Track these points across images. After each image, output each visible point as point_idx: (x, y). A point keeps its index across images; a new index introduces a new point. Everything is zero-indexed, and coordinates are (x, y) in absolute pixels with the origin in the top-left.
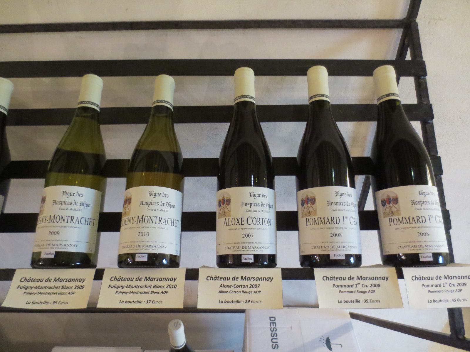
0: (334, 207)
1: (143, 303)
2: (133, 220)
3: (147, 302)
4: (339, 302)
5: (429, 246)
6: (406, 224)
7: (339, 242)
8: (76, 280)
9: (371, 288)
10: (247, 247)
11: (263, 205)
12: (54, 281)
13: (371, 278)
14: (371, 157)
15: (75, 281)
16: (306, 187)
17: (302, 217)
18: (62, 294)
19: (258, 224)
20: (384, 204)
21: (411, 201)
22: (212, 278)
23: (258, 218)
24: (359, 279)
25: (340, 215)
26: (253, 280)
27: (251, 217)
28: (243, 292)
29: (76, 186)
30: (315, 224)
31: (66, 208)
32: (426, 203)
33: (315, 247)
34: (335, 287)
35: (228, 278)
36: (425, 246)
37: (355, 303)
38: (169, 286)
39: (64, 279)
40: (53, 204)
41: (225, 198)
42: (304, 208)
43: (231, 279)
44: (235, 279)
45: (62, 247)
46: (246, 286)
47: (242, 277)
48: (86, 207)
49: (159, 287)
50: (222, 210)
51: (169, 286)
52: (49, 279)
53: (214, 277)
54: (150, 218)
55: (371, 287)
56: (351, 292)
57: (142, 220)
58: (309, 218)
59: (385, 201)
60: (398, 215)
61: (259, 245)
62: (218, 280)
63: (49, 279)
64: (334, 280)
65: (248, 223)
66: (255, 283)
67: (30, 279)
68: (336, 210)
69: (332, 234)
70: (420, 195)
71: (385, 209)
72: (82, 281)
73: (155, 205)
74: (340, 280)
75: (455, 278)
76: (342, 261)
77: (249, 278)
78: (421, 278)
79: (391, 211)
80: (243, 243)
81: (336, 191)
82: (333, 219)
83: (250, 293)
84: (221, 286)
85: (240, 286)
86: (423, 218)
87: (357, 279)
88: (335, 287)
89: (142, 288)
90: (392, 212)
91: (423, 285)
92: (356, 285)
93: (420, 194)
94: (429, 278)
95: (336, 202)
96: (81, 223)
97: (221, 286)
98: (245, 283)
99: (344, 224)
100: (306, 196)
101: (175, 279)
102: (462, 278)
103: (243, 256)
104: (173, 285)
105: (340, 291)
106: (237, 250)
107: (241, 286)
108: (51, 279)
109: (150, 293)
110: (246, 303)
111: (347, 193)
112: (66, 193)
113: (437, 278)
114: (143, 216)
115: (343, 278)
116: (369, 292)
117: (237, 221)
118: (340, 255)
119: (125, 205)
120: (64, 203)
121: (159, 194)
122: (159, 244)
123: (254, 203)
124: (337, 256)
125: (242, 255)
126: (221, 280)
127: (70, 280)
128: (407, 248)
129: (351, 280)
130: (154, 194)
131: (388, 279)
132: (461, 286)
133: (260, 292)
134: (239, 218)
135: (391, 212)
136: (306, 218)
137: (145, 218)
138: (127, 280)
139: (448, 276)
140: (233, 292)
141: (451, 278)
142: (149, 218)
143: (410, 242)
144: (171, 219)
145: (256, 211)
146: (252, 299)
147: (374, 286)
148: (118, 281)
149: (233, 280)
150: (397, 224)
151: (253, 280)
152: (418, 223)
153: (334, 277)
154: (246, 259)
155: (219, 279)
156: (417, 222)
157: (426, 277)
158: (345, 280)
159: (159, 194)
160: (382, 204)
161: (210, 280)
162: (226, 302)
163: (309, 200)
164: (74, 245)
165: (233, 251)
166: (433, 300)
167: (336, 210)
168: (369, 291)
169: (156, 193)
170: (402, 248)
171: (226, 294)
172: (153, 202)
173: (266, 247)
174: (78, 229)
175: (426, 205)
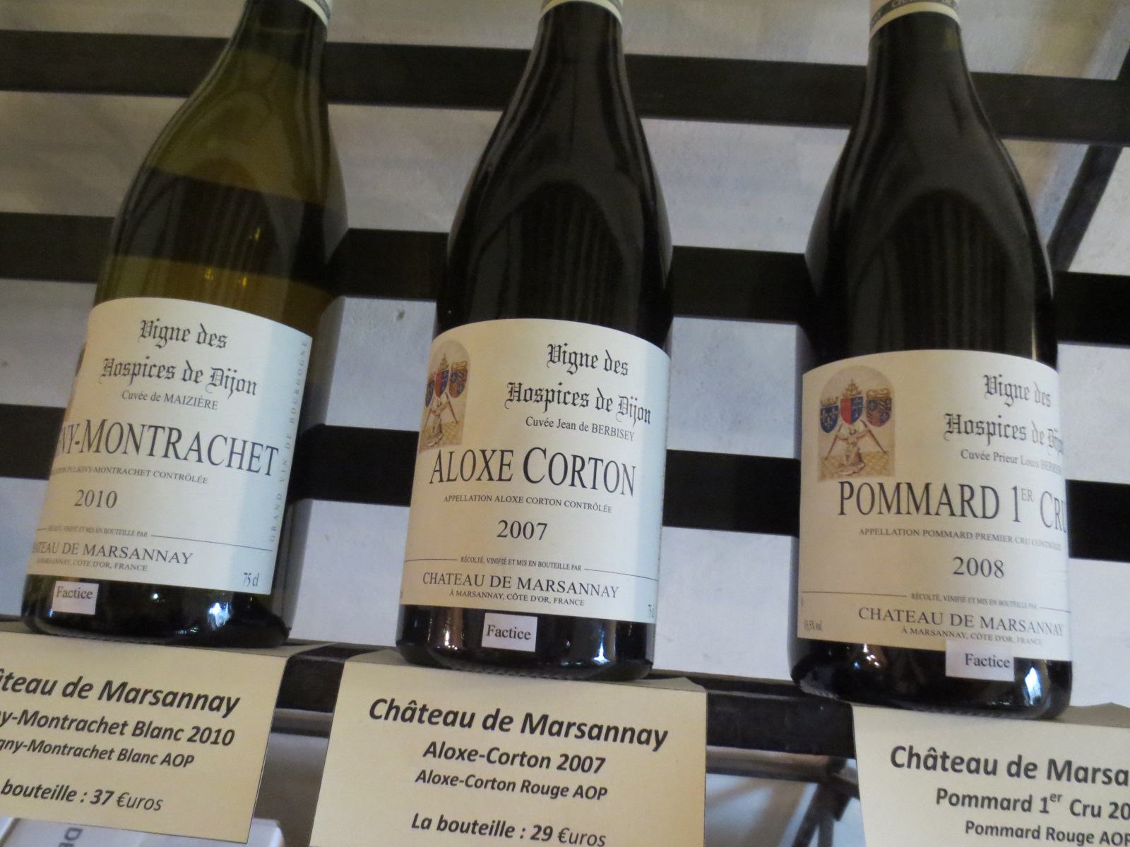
0: (977, 443)
1: (77, 799)
3: (98, 797)
5: (532, 586)
6: (908, 513)
7: (993, 602)
12: (100, 698)
13: (1112, 775)
17: (823, 477)
18: (138, 758)
19: (573, 484)
21: (948, 415)
22: (393, 712)
23: (575, 457)
24: (1059, 777)
25: (1002, 477)
26: (576, 737)
27: (544, 452)
28: (526, 786)
30: (884, 509)
31: (578, 424)
32: (1009, 431)
33: (876, 614)
34: (947, 800)
38: (200, 735)
39: (146, 692)
41: (450, 368)
42: (835, 440)
43: (1002, 769)
44: (497, 721)
46: (543, 759)
49: (156, 732)
50: (432, 415)
51: (200, 735)
53: (407, 706)
54: (131, 429)
55: (1112, 816)
56: (1020, 833)
57: (100, 438)
58: (857, 482)
59: (836, 408)
60: (880, 473)
62: (420, 721)
64: (945, 769)
65: (213, 463)
66: (586, 748)
69: (506, 524)
70: (988, 395)
74: (970, 771)
75: (1100, 776)
77: (561, 724)
79: (856, 449)
82: (967, 495)
83: (557, 792)
84: (431, 750)
85: (515, 756)
86: (990, 495)
87: (1049, 777)
88: (947, 800)
89: (83, 729)
90: (859, 457)
91: (942, 794)
92: (1045, 800)
93: (989, 392)
94: (973, 766)
95: (985, 420)
97: (431, 750)
98: (539, 744)
99: (1017, 520)
100: (441, 364)
101: (232, 702)
103: (489, 619)
104: (219, 731)
105: (970, 826)
106: (467, 588)
107: (518, 760)
109: (115, 756)
110: (533, 838)
111: (1032, 389)
112: (156, 327)
117: (484, 465)
118: (994, 663)
119: (434, 395)
120: (556, 399)
122: (141, 544)
123: (564, 389)
124: (980, 663)
125: (487, 615)
127: (170, 699)
130: (158, 330)
133: (601, 793)
134: (494, 451)
136: (842, 483)
137: (110, 430)
138: (28, 691)
139: (1069, 764)
140: (481, 784)
141: (1084, 775)
142: (126, 429)
143: (914, 596)
144: (230, 441)
145: (571, 426)
147: (575, 765)
149: (485, 727)
151: (576, 737)
152: (963, 515)
153: (945, 753)
154: (500, 634)
156: (957, 510)
157: (962, 760)
158: (994, 772)
159: (590, 358)
160: (821, 420)
161: (386, 718)
162: (443, 825)
168: (1105, 834)
171: (448, 788)
172: (150, 362)
173: (601, 590)
175: (155, 379)
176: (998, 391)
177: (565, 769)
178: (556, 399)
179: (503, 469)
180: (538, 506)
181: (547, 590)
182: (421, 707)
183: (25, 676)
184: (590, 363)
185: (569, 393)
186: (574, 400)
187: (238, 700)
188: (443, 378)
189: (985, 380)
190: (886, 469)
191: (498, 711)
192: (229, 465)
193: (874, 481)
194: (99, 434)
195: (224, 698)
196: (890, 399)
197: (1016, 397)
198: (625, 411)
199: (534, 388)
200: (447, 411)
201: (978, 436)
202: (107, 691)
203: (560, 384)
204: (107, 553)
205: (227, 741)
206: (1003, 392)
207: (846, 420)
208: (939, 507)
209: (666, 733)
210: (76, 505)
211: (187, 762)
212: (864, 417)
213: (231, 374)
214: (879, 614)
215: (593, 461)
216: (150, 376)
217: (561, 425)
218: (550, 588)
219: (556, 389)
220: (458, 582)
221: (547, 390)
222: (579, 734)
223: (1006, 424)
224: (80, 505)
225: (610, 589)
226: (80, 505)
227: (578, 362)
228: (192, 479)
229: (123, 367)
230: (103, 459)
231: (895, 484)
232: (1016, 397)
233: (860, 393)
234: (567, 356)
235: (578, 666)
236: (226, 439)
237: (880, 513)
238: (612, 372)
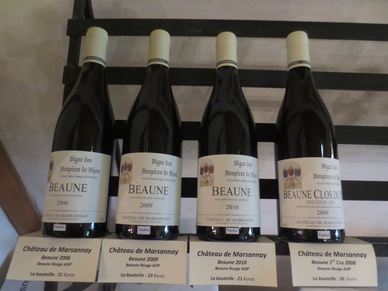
4: (314, 280)
5: (236, 220)
8: (82, 250)
9: (346, 265)
10: (232, 220)
11: (248, 175)
14: (276, 124)
15: (81, 251)
16: (206, 154)
20: (285, 175)
21: (314, 174)
22: (203, 254)
27: (319, 191)
29: (162, 153)
31: (75, 176)
32: (240, 174)
35: (131, 250)
36: (323, 222)
37: (330, 280)
40: (61, 171)
41: (208, 166)
43: (223, 255)
45: (71, 218)
47: (234, 253)
48: (95, 173)
52: (53, 249)
53: (118, 249)
59: (287, 172)
61: (244, 218)
63: (53, 249)
65: (316, 198)
67: (34, 248)
68: (322, 184)
71: (202, 177)
72: (88, 252)
73: (241, 175)
78: (308, 253)
79: (292, 182)
80: (140, 213)
81: (322, 163)
87: (233, 256)
90: (294, 184)
96: (298, 198)
102: (353, 256)
103: (227, 228)
104: (243, 261)
106: (133, 220)
108: (56, 249)
110: (238, 280)
111: (247, 163)
112: (238, 163)
113: (326, 255)
115: (320, 254)
116: (345, 269)
120: (237, 174)
121: (162, 162)
126: (213, 256)
128: (305, 223)
129: (139, 252)
131: (367, 256)
132: (349, 264)
135: (206, 182)
146: (155, 274)
148: (118, 252)
150: (328, 198)
155: (211, 254)
160: (284, 174)
163: (127, 166)
164: (84, 215)
165: (216, 223)
166: (319, 277)
167: (322, 184)
169: (241, 162)
170: (300, 223)
173: (166, 219)
175: (240, 176)
176: (238, 164)
178: (237, 174)
179: (249, 194)
180: (76, 197)
183: (40, 247)
184: (244, 165)
186: (158, 173)
187: (91, 250)
188: (126, 166)
190: (300, 187)
191: (139, 249)
196: (213, 167)
197: (160, 164)
198: (91, 171)
199: (232, 172)
200: (127, 175)
202: (234, 254)
204: (67, 216)
206: (239, 164)
207: (205, 172)
208: (60, 189)
210: (58, 204)
211: (247, 269)
212: (208, 171)
213: (94, 169)
214: (211, 219)
216: (156, 174)
217: (242, 181)
219: (237, 172)
222: (246, 256)
223: (239, 172)
224: (58, 204)
229: (149, 171)
232: (160, 164)
233: (293, 168)
235: (333, 241)
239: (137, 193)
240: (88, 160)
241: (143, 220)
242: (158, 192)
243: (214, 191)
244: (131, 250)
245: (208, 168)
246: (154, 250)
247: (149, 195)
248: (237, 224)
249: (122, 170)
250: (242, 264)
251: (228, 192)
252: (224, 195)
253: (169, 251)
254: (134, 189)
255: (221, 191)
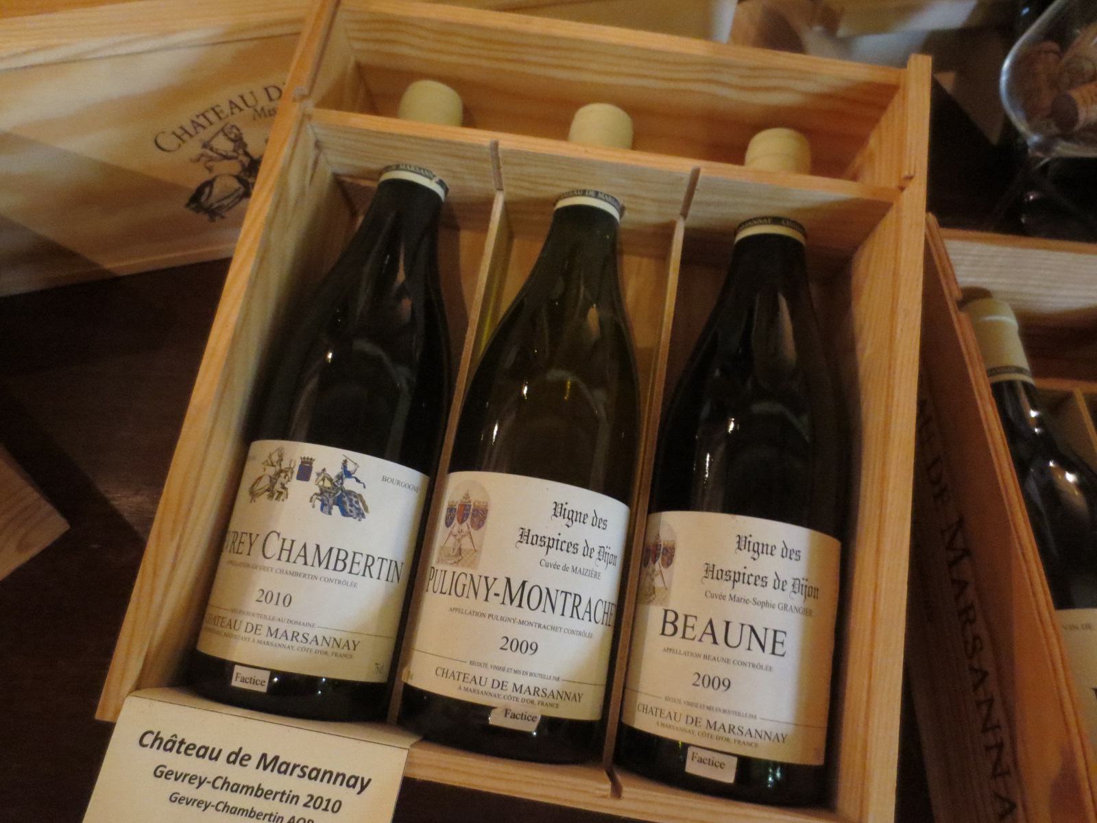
2: (488, 590)
6: (312, 566)
27: (279, 535)
35: (214, 749)
41: (472, 504)
53: (169, 738)
62: (178, 752)
70: (554, 517)
73: (568, 551)
76: (523, 735)
77: (288, 765)
80: (498, 668)
95: (547, 535)
104: (329, 801)
106: (472, 686)
114: (524, 583)
119: (643, 568)
123: (561, 538)
125: (236, 666)
135: (456, 551)
137: (531, 590)
148: (165, 749)
149: (228, 761)
151: (299, 776)
155: (183, 748)
161: (152, 746)
169: (760, 542)
172: (748, 572)
174: (588, 639)
177: (309, 807)
181: (534, 695)
182: (180, 740)
184: (582, 520)
185: (752, 575)
186: (568, 547)
189: (738, 539)
190: (473, 564)
192: (279, 559)
193: (469, 571)
194: (520, 591)
195: (358, 777)
198: (601, 558)
199: (540, 535)
200: (659, 576)
201: (725, 582)
203: (745, 568)
205: (335, 809)
207: (458, 521)
209: (369, 781)
212: (468, 521)
215: (380, 560)
218: (536, 694)
219: (742, 572)
220: (466, 680)
221: (549, 538)
224: (698, 685)
225: (577, 696)
226: (698, 685)
227: (760, 551)
228: (761, 667)
229: (539, 539)
230: (525, 613)
231: (521, 582)
234: (752, 545)
236: (466, 575)
237: (503, 603)
238: (596, 527)
239: (350, 572)
240: (772, 547)
241: (696, 729)
242: (379, 574)
243: (665, 622)
244: (214, 749)
245: (471, 510)
246: (207, 745)
247: (721, 648)
248: (719, 738)
249: (447, 518)
250: (325, 812)
251: (704, 633)
252: (691, 639)
253: (338, 775)
254: (346, 561)
255: (685, 626)
